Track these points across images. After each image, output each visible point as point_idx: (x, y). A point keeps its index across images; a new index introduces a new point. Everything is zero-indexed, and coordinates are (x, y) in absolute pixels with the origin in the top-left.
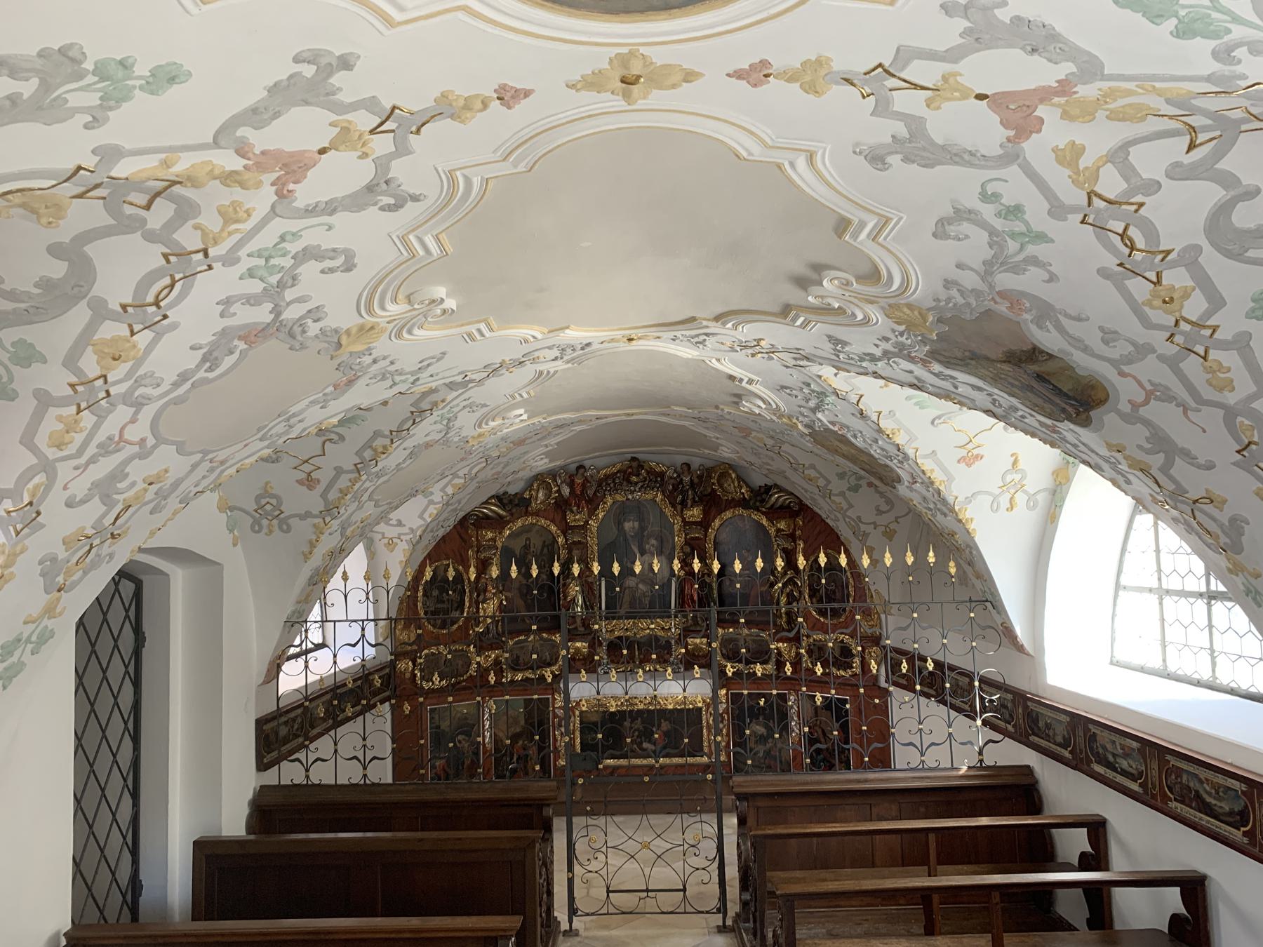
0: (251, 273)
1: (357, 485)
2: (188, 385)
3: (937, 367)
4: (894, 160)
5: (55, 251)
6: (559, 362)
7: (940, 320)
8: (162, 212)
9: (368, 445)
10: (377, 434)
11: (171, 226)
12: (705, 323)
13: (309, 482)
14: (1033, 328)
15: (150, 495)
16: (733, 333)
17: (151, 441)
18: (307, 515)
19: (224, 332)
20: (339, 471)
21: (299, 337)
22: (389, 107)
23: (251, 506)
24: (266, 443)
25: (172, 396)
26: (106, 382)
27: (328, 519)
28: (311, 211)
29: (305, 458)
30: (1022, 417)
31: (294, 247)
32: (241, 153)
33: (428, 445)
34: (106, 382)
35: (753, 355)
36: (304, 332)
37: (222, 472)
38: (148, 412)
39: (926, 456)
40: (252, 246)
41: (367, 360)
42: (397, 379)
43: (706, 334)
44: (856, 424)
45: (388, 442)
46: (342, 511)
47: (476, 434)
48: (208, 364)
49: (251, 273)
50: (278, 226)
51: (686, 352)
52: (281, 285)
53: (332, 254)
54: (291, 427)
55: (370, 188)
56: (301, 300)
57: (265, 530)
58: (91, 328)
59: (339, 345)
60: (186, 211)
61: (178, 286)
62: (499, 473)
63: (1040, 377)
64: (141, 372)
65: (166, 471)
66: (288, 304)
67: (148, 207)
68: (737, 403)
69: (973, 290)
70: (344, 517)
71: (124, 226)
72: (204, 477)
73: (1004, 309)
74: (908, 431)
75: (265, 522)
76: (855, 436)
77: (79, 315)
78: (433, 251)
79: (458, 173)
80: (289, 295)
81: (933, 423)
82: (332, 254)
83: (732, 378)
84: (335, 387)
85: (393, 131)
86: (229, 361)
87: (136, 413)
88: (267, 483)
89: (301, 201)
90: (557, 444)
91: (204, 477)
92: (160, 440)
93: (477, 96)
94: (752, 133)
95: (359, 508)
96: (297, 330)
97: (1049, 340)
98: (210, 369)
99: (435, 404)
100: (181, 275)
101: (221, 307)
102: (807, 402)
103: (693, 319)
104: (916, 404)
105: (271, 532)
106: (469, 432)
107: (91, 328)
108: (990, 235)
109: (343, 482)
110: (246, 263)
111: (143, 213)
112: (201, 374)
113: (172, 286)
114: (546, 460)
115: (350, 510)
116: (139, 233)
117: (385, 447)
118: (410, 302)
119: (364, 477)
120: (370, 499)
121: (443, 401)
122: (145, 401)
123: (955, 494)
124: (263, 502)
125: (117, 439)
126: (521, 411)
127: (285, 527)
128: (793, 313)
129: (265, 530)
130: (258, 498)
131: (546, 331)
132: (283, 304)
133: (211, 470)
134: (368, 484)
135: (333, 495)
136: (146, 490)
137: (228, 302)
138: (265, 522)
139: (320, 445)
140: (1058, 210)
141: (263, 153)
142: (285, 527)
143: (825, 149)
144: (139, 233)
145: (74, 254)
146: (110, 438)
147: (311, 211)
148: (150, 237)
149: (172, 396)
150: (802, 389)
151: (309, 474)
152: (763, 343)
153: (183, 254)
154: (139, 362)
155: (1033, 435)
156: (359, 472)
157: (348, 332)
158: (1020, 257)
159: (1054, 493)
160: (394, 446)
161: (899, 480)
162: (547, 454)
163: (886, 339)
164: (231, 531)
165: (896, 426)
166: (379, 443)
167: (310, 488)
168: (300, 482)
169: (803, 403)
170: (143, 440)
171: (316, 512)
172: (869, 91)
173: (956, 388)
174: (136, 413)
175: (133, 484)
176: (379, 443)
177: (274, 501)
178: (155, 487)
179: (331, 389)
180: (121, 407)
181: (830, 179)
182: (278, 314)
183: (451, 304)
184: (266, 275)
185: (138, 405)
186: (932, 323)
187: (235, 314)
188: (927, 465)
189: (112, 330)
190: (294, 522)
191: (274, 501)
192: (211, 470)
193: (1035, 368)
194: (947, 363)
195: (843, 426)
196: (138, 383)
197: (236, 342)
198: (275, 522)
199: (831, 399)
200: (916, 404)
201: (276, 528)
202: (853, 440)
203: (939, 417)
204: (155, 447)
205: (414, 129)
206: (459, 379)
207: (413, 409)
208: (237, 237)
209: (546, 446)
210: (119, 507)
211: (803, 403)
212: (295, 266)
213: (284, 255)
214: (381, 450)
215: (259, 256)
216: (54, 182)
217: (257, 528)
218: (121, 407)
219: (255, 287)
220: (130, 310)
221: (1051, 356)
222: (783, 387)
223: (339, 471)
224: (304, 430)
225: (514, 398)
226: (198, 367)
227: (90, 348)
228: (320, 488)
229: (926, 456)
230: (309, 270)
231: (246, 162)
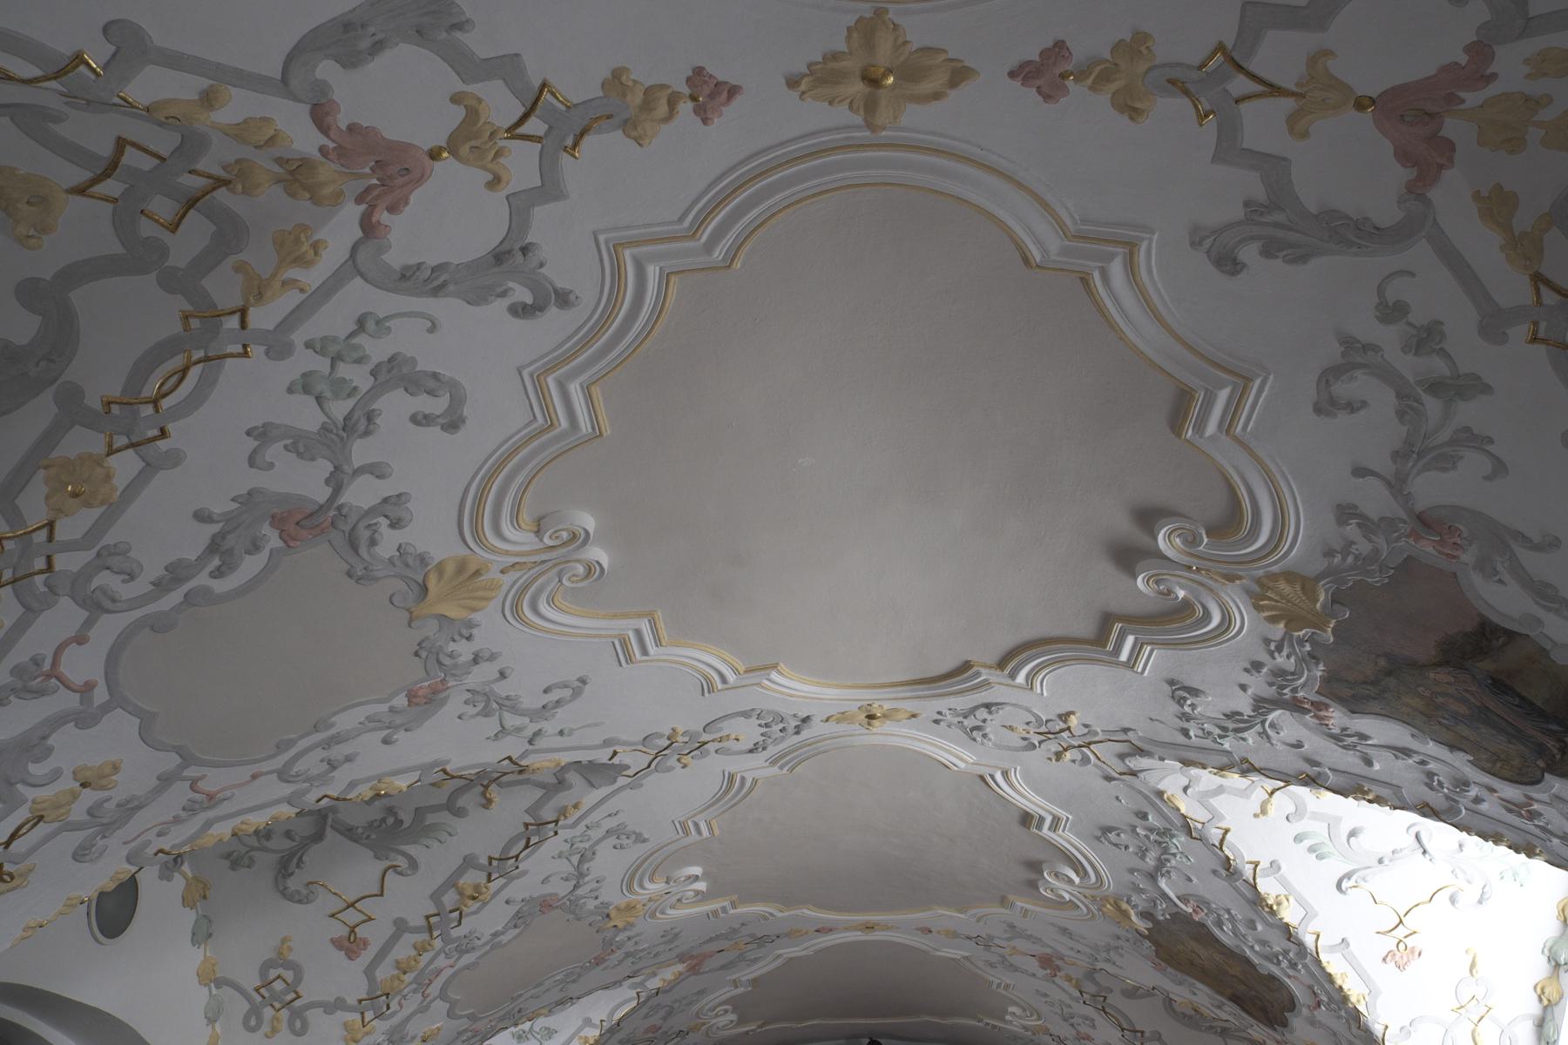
0: (305, 385)
1: (426, 957)
2: (175, 597)
3: (1337, 717)
4: (1249, 254)
5: (28, 293)
6: (760, 758)
7: (1335, 600)
8: (196, 233)
9: (451, 883)
10: (469, 862)
11: (206, 262)
12: (985, 675)
13: (350, 944)
14: (1476, 579)
15: (78, 813)
16: (1024, 698)
17: (101, 695)
18: (338, 1005)
19: (249, 499)
20: (401, 927)
21: (363, 551)
22: (537, 84)
23: (251, 980)
24: (287, 789)
25: (151, 608)
26: (50, 538)
27: (369, 1015)
28: (407, 279)
29: (351, 900)
30: (1478, 800)
31: (377, 349)
32: (321, 115)
33: (546, 904)
34: (50, 538)
35: (1059, 756)
36: (373, 542)
37: (208, 825)
38: (109, 628)
39: (1332, 949)
40: (314, 327)
41: (464, 650)
42: (511, 721)
43: (988, 706)
44: (1217, 892)
45: (481, 877)
46: (394, 1005)
47: (622, 902)
48: (216, 562)
49: (305, 385)
50: (358, 296)
51: (959, 755)
52: (348, 425)
53: (431, 384)
54: (333, 766)
55: (499, 256)
56: (377, 471)
57: (266, 1028)
58: (49, 439)
59: (424, 589)
60: (229, 235)
61: (194, 373)
62: (655, 1029)
63: (1499, 685)
64: (109, 539)
65: (116, 768)
66: (358, 472)
67: (174, 227)
68: (1033, 885)
69: (1382, 519)
70: (395, 1020)
71: (138, 257)
72: (177, 820)
73: (1430, 549)
74: (1301, 902)
75: (268, 1012)
76: (1220, 924)
77: (40, 412)
78: (582, 425)
79: (627, 253)
80: (361, 451)
81: (1339, 886)
82: (431, 384)
83: (1026, 819)
84: (411, 696)
85: (538, 139)
86: (251, 566)
87: (88, 624)
88: (284, 940)
89: (396, 258)
90: (754, 982)
91: (177, 820)
92: (117, 699)
93: (663, 87)
94: (1045, 205)
95: (422, 1009)
96: (364, 535)
97: (1504, 601)
98: (218, 574)
99: (563, 812)
100: (201, 354)
101: (252, 444)
102: (1143, 857)
103: (966, 666)
104: (1311, 849)
105: (274, 1031)
106: (612, 895)
107: (49, 439)
108: (1399, 396)
109: (403, 950)
110: (304, 361)
111: (166, 236)
112: (202, 579)
113: (184, 371)
114: (733, 1017)
115: (406, 1012)
116: (154, 275)
117: (477, 888)
118: (538, 532)
119: (438, 943)
120: (443, 996)
121: (576, 806)
122: (107, 604)
123: (1383, 1020)
124: (273, 974)
125: (47, 667)
126: (696, 870)
127: (298, 1024)
128: (1118, 626)
129: (266, 1028)
130: (267, 966)
131: (742, 668)
132: (346, 468)
133: (191, 809)
134: (441, 961)
135: (384, 972)
136: (75, 796)
137: (263, 434)
138: (268, 1012)
139: (378, 875)
140: (1493, 324)
141: (352, 128)
142: (298, 1024)
143: (1151, 240)
144: (154, 275)
145: (48, 297)
146: (36, 661)
147: (407, 279)
148: (171, 282)
149: (151, 608)
150: (1134, 828)
151: (352, 930)
152: (1074, 721)
153: (213, 316)
154: (114, 510)
155: (1497, 839)
156: (430, 929)
157: (440, 568)
158: (1445, 435)
159: (1541, 1024)
160: (494, 886)
161: (1291, 1004)
162: (736, 1004)
163: (1257, 666)
164: (211, 1021)
165: (1283, 892)
166: (472, 878)
167: (351, 955)
168: (337, 943)
169: (1137, 862)
170: (89, 687)
171: (351, 1000)
172: (1208, 107)
173: (1369, 763)
174: (88, 624)
175: (56, 774)
176: (472, 878)
177: (289, 975)
178: (89, 797)
179: (401, 701)
180: (65, 602)
181: (1161, 308)
182: (337, 491)
183: (598, 554)
184: (328, 394)
185: (97, 606)
186: (1324, 606)
187: (271, 465)
188: (1334, 964)
189: (81, 442)
190: (314, 1016)
191: (289, 975)
192: (191, 809)
193: (1486, 665)
194: (1355, 705)
195: (1202, 903)
196: (102, 562)
197: (266, 529)
198: (284, 1013)
199: (1180, 840)
200: (1311, 849)
201: (284, 1026)
202: (1216, 931)
203: (1348, 876)
204: (106, 708)
205: (569, 142)
206: (602, 756)
207: (529, 819)
208: (292, 299)
209: (735, 984)
210: (22, 814)
211: (1137, 862)
212: (376, 392)
213: (359, 361)
214: (469, 892)
215: (322, 352)
216: (38, 73)
217: (253, 1023)
218: (65, 602)
219: (306, 416)
220: (115, 409)
221: (1511, 635)
222: (1107, 830)
223: (401, 927)
224: (352, 785)
225: (686, 833)
226: (202, 560)
227: (41, 473)
228: (366, 957)
229: (1332, 949)
230: (395, 406)
231: (325, 141)
